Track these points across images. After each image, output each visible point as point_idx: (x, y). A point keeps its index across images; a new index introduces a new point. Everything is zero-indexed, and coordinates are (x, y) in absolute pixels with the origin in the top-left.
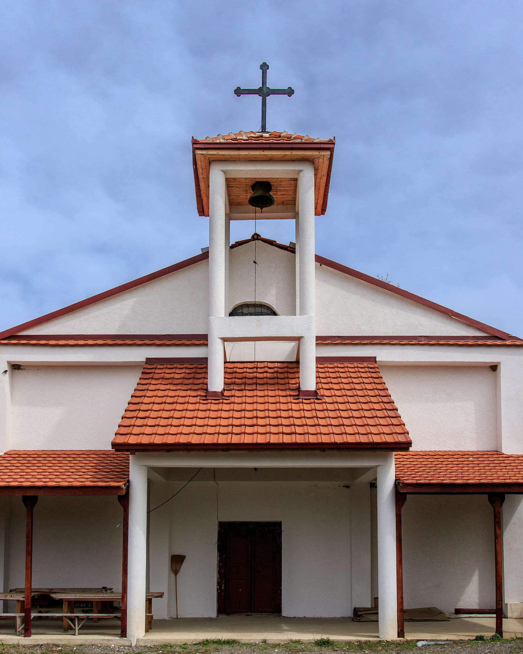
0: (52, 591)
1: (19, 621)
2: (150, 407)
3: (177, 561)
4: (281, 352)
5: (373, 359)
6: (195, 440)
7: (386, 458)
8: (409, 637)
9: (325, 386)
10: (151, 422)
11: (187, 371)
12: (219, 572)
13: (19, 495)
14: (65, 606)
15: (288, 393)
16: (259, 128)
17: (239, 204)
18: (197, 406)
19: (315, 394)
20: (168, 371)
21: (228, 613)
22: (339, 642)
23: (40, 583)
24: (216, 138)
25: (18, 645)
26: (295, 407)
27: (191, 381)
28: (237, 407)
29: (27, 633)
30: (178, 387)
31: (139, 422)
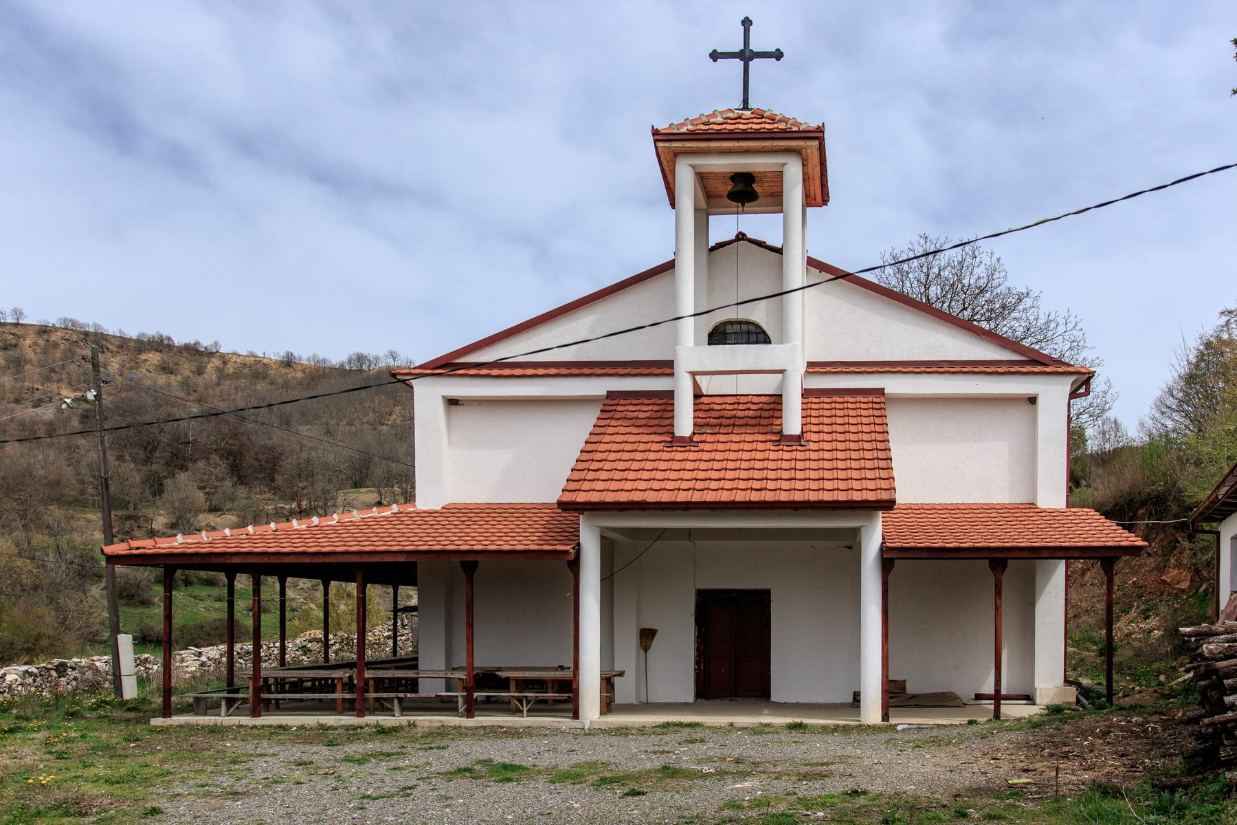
0: (499, 669)
1: (460, 701)
2: (604, 456)
3: (647, 636)
4: (766, 385)
5: (880, 392)
6: (651, 497)
7: (871, 518)
8: (893, 721)
9: (814, 428)
10: (604, 475)
11: (655, 408)
12: (698, 649)
13: (456, 560)
14: (512, 685)
15: (768, 437)
16: (738, 103)
17: (718, 196)
18: (659, 455)
19: (798, 439)
20: (632, 408)
21: (708, 698)
22: (813, 726)
23: (483, 661)
24: (682, 125)
25: (460, 727)
26: (773, 455)
27: (656, 422)
28: (706, 456)
29: (469, 713)
30: (641, 430)
31: (591, 475)
